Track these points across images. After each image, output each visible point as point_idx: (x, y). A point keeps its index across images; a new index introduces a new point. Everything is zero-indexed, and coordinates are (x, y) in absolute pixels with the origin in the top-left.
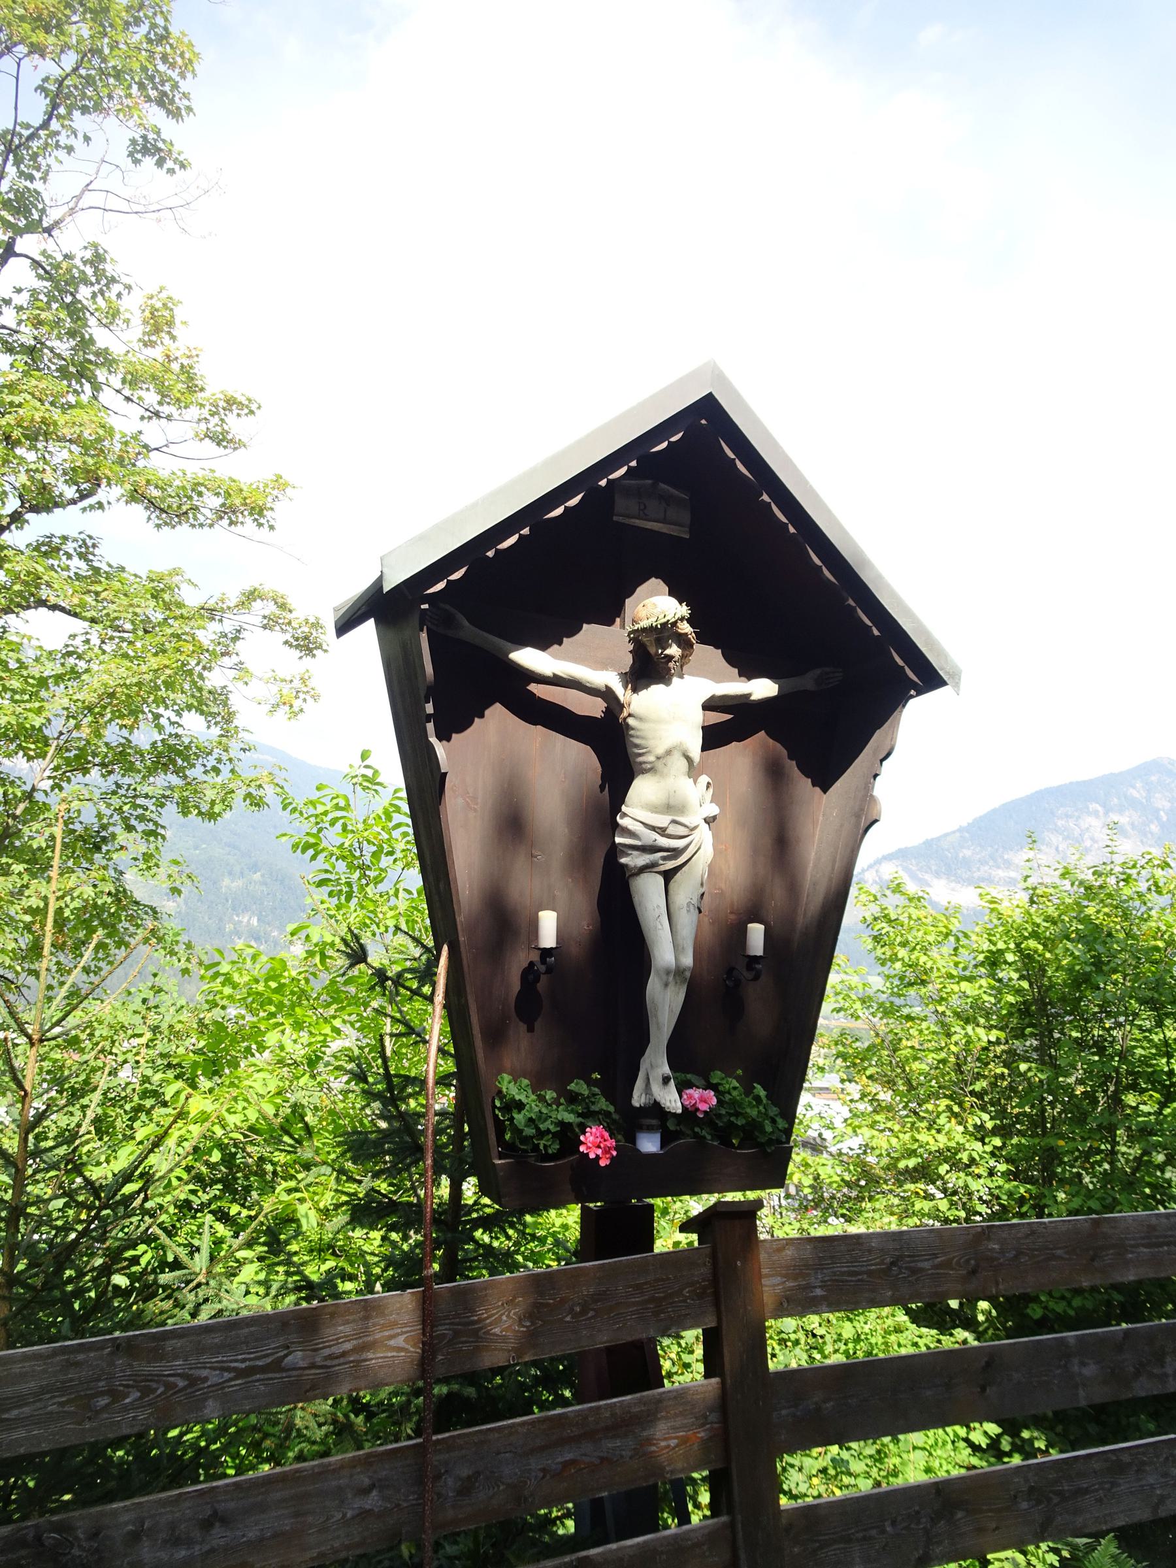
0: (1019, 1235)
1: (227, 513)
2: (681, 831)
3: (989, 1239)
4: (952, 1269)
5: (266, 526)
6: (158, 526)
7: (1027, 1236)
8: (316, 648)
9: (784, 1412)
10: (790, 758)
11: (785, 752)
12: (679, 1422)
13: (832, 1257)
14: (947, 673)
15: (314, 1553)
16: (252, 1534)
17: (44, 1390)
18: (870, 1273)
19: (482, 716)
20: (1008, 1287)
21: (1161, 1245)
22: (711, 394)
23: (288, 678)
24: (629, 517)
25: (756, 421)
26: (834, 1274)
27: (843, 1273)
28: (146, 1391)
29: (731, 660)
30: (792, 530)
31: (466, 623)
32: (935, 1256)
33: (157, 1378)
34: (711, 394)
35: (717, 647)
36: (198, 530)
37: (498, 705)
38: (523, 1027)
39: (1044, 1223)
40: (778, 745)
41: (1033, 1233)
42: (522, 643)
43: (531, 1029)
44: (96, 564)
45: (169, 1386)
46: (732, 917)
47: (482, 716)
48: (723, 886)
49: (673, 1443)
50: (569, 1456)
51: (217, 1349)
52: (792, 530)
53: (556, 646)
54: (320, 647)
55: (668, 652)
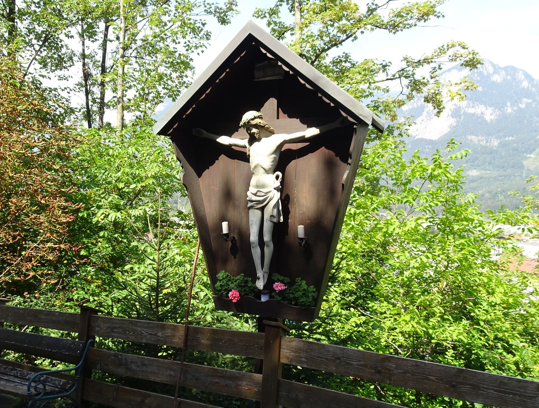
0: (409, 364)
1: (424, 17)
2: (262, 194)
3: (390, 361)
4: (367, 368)
5: (441, 16)
6: (394, 33)
7: (413, 366)
8: (478, 64)
9: (284, 393)
10: (337, 156)
11: (334, 154)
12: (249, 383)
13: (311, 349)
14: (363, 116)
15: (160, 379)
16: (150, 370)
17: (120, 327)
18: (327, 359)
19: (218, 159)
20: (168, 345)
21: (509, 393)
22: (250, 34)
23: (459, 82)
24: (259, 78)
25: (218, 58)
26: (312, 355)
27: (315, 356)
28: (134, 333)
29: (303, 122)
30: (194, 106)
31: (205, 132)
32: (360, 361)
33: (136, 330)
34: (250, 34)
35: (297, 118)
36: (410, 29)
37: (223, 155)
38: (233, 257)
39: (425, 363)
40: (331, 152)
41: (417, 365)
42: (220, 135)
43: (235, 257)
44: (353, 62)
45: (138, 333)
46: (308, 221)
47: (218, 159)
48: (304, 210)
49: (246, 388)
50: (217, 381)
51: (146, 328)
52: (194, 106)
53: (236, 132)
54: (479, 63)
55: (252, 131)
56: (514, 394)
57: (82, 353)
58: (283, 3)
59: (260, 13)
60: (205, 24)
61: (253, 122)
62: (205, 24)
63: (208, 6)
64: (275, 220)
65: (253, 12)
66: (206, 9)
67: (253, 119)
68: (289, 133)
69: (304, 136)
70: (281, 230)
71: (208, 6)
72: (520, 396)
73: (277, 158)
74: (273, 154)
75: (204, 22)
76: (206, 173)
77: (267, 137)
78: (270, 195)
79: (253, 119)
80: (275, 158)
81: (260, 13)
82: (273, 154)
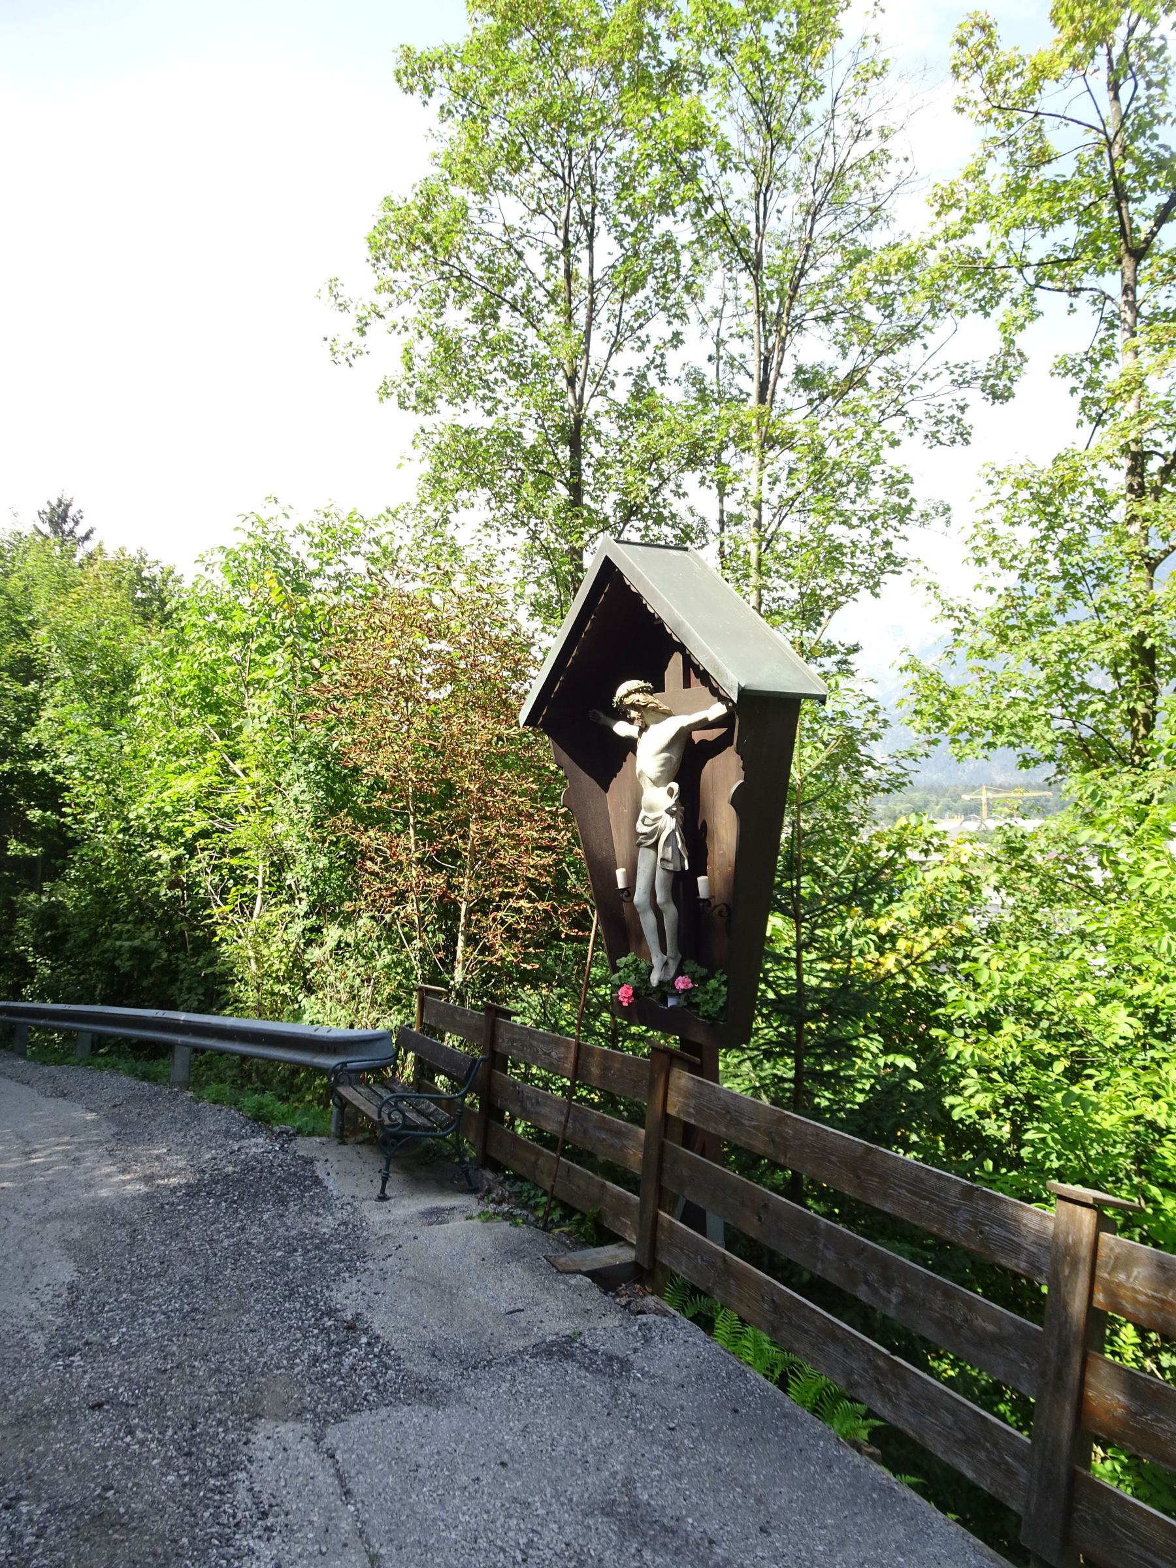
21: (925, 1198)
56: (932, 1201)
57: (468, 1075)
58: (1116, 331)
59: (1070, 364)
60: (966, 405)
61: (628, 701)
62: (966, 405)
63: (958, 371)
64: (671, 867)
65: (1051, 367)
66: (955, 377)
67: (626, 696)
68: (689, 713)
69: (706, 720)
70: (682, 884)
71: (958, 371)
72: (938, 1204)
73: (675, 758)
74: (663, 751)
75: (962, 404)
76: (614, 784)
77: (657, 722)
78: (660, 824)
79: (626, 696)
80: (668, 760)
81: (1070, 364)
82: (663, 751)
